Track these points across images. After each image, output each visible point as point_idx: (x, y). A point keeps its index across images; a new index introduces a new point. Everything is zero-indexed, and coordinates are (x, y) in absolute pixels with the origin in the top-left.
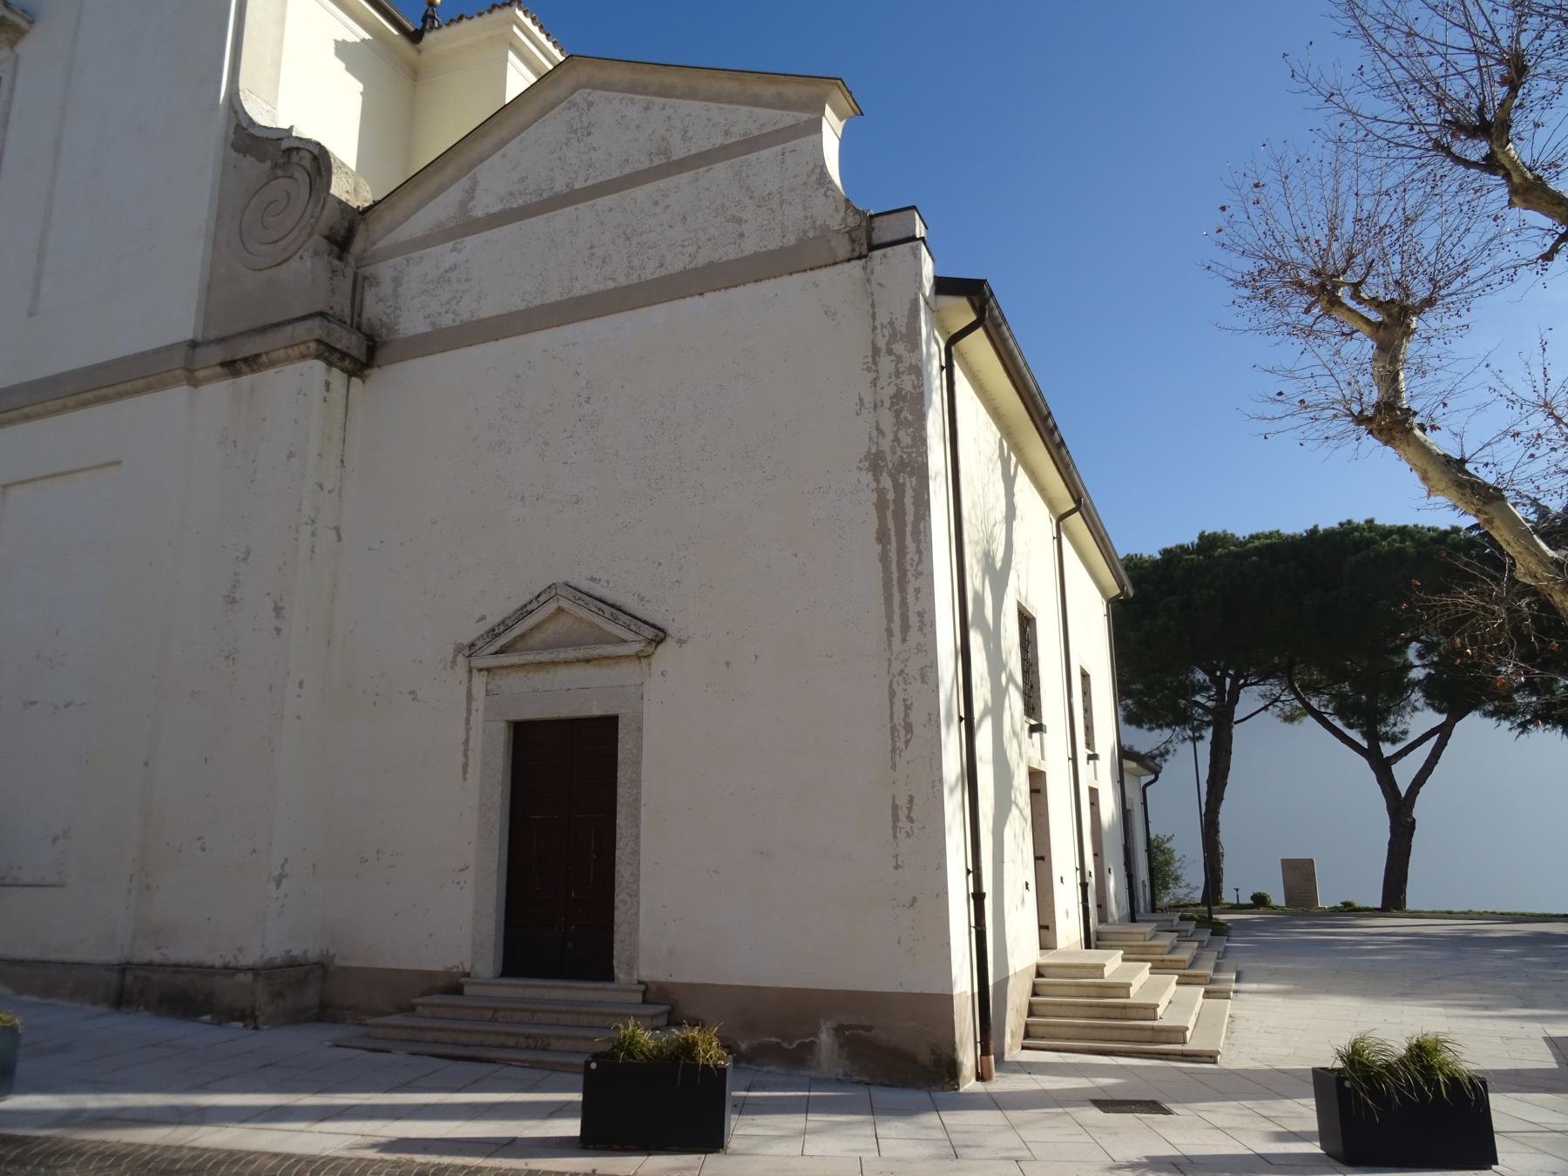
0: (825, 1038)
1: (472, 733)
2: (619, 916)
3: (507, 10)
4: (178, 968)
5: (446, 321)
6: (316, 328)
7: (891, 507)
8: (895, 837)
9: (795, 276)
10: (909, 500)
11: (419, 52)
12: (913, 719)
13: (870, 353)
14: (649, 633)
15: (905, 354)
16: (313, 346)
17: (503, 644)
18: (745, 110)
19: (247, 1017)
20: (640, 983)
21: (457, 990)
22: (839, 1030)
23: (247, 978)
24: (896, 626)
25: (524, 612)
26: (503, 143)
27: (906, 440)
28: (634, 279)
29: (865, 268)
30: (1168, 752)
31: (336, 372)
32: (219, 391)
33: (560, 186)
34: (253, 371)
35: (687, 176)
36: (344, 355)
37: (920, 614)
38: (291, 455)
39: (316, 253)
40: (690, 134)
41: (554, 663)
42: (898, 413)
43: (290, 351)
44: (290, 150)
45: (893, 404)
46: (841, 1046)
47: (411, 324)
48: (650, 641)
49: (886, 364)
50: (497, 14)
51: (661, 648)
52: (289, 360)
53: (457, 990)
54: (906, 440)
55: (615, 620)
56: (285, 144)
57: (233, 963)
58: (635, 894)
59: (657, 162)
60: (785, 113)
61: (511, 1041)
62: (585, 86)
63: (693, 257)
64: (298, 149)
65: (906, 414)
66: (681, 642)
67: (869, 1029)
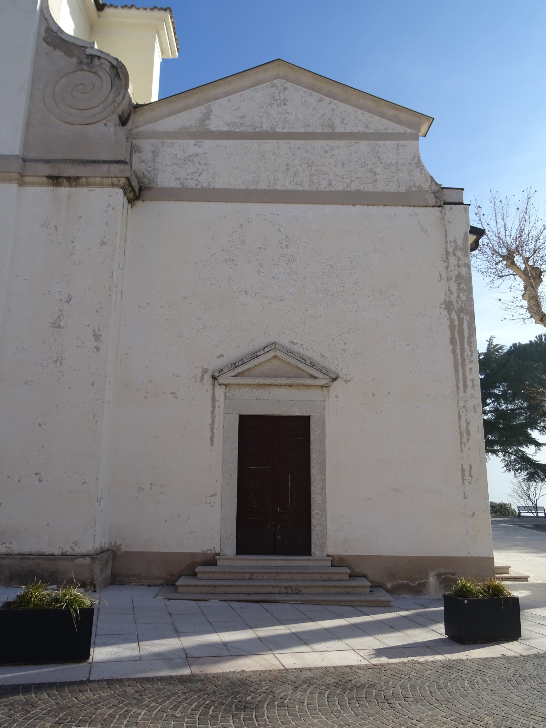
0: (432, 580)
1: (216, 420)
4: (23, 556)
5: (191, 184)
7: (457, 328)
8: (463, 484)
9: (405, 207)
11: (99, 16)
13: (445, 253)
15: (462, 257)
16: (123, 181)
18: (377, 118)
20: (328, 556)
22: (439, 576)
24: (461, 384)
25: (255, 355)
26: (229, 94)
27: (464, 298)
29: (441, 212)
32: (40, 195)
33: (266, 126)
34: (71, 186)
35: (344, 143)
38: (103, 243)
40: (345, 121)
41: (271, 385)
42: (459, 285)
43: (105, 180)
44: (92, 57)
45: (456, 280)
46: (440, 583)
47: (166, 179)
49: (453, 260)
50: (156, 13)
51: (335, 383)
52: (102, 185)
54: (464, 298)
56: (89, 51)
57: (70, 552)
58: (324, 510)
59: (326, 130)
60: (399, 126)
61: (276, 590)
62: (282, 78)
63: (348, 185)
64: (99, 57)
65: (462, 285)
66: (346, 381)
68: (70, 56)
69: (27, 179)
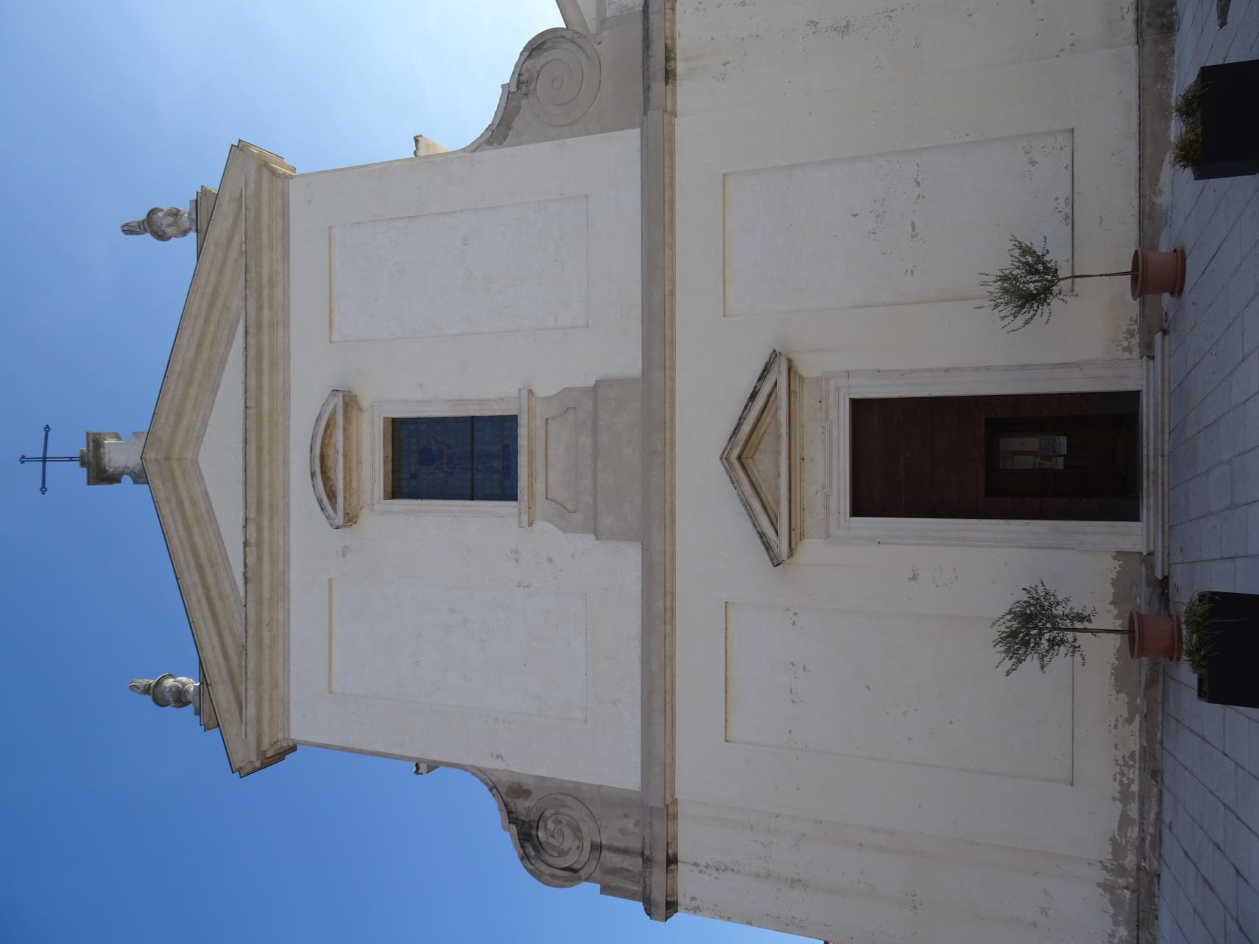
34: (675, 59)
43: (668, 17)
44: (519, 83)
52: (673, 22)
56: (513, 89)
68: (520, 107)
69: (669, 107)
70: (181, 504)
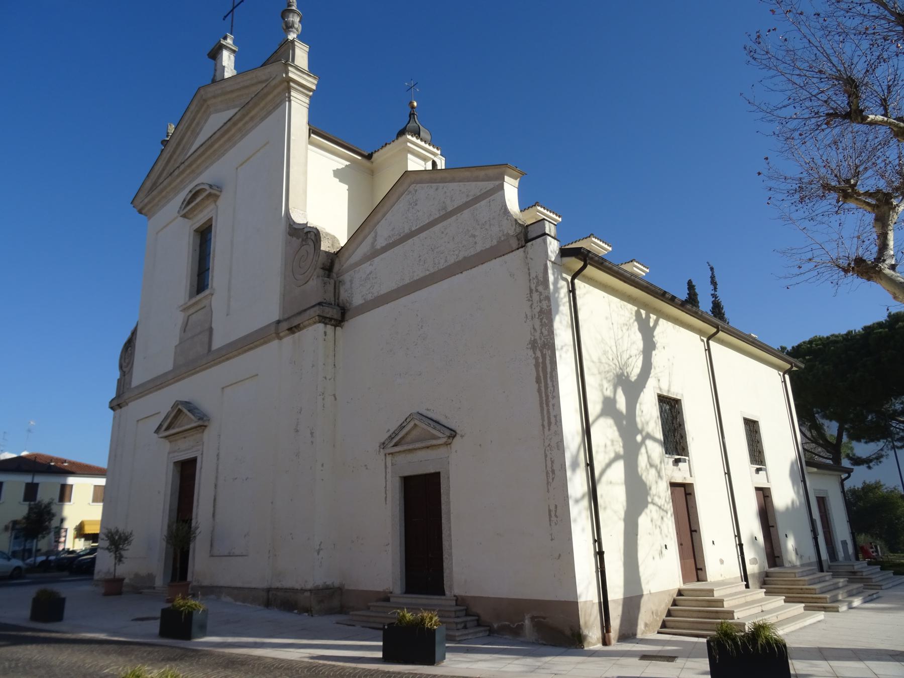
0: (527, 622)
2: (445, 565)
3: (404, 137)
4: (286, 590)
5: (369, 297)
6: (317, 311)
10: (548, 362)
12: (555, 468)
14: (448, 433)
17: (397, 441)
19: (308, 610)
21: (387, 599)
23: (307, 594)
24: (546, 423)
25: (402, 427)
26: (384, 216)
27: (546, 333)
28: (436, 269)
30: (882, 456)
31: (329, 326)
32: (288, 340)
36: (331, 319)
37: (555, 416)
38: (313, 366)
39: (318, 277)
42: (541, 320)
47: (357, 300)
48: (449, 437)
49: (536, 296)
52: (310, 325)
53: (387, 599)
54: (546, 333)
55: (435, 428)
56: (306, 230)
59: (442, 213)
63: (458, 256)
65: (544, 320)
66: (462, 436)
67: (544, 618)
70: (194, 119)
